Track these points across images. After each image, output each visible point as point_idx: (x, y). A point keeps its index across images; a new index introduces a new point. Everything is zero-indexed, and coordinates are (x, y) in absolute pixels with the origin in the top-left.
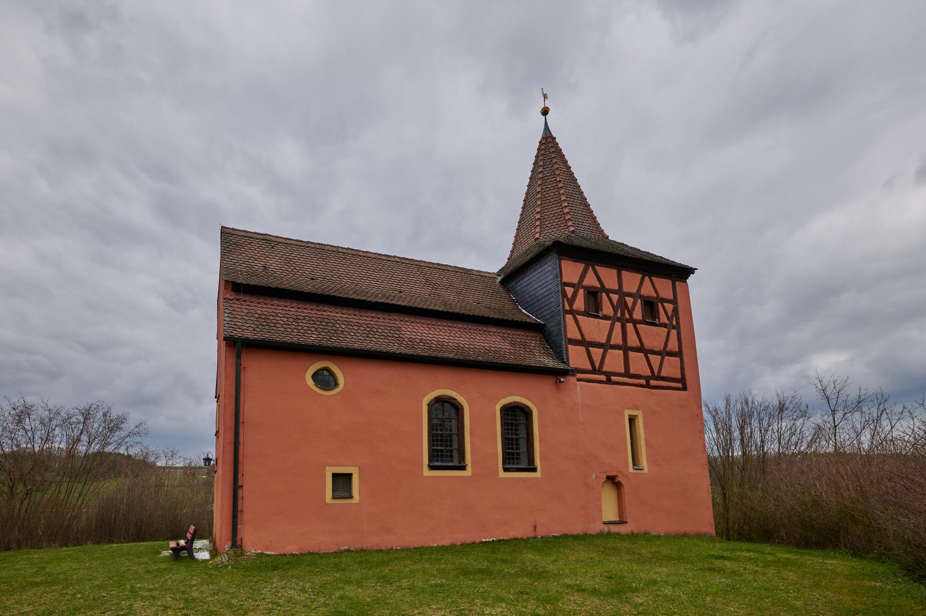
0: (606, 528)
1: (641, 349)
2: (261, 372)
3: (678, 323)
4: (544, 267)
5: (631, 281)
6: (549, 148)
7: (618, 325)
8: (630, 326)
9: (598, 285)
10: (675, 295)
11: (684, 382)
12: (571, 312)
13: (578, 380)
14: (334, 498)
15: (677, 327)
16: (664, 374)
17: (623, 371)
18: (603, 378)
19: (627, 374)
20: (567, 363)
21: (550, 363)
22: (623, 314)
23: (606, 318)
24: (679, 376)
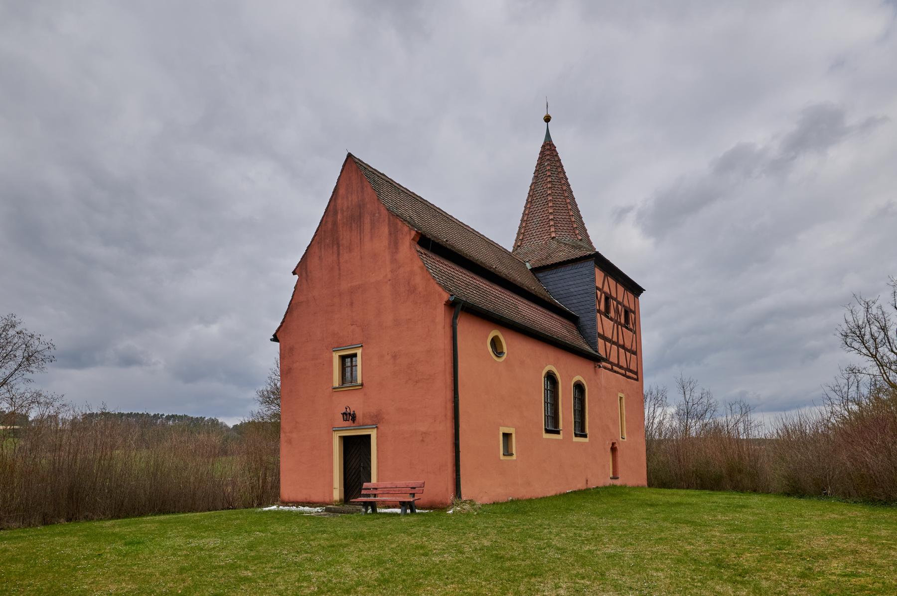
1: (623, 347)
6: (549, 151)
15: (635, 333)
18: (609, 366)
19: (618, 365)
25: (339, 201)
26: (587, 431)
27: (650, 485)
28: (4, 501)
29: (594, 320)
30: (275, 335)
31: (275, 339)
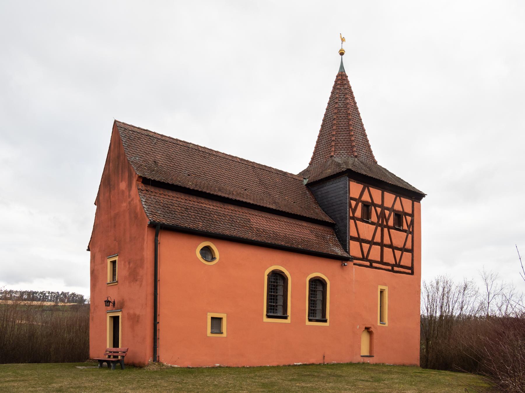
0: (362, 360)
1: (391, 246)
2: (169, 244)
3: (413, 230)
4: (339, 184)
5: (389, 198)
6: (342, 82)
7: (379, 229)
8: (386, 230)
9: (369, 200)
10: (413, 211)
11: (412, 270)
12: (354, 218)
13: (355, 264)
14: (212, 333)
15: (412, 233)
16: (402, 263)
17: (379, 260)
18: (368, 263)
19: (382, 262)
20: (348, 253)
21: (339, 251)
22: (383, 222)
23: (373, 223)
24: (410, 265)
25: (111, 154)
26: (328, 317)
27: (421, 366)
28: (3, 325)
29: (346, 226)
30: (88, 247)
31: (88, 250)
